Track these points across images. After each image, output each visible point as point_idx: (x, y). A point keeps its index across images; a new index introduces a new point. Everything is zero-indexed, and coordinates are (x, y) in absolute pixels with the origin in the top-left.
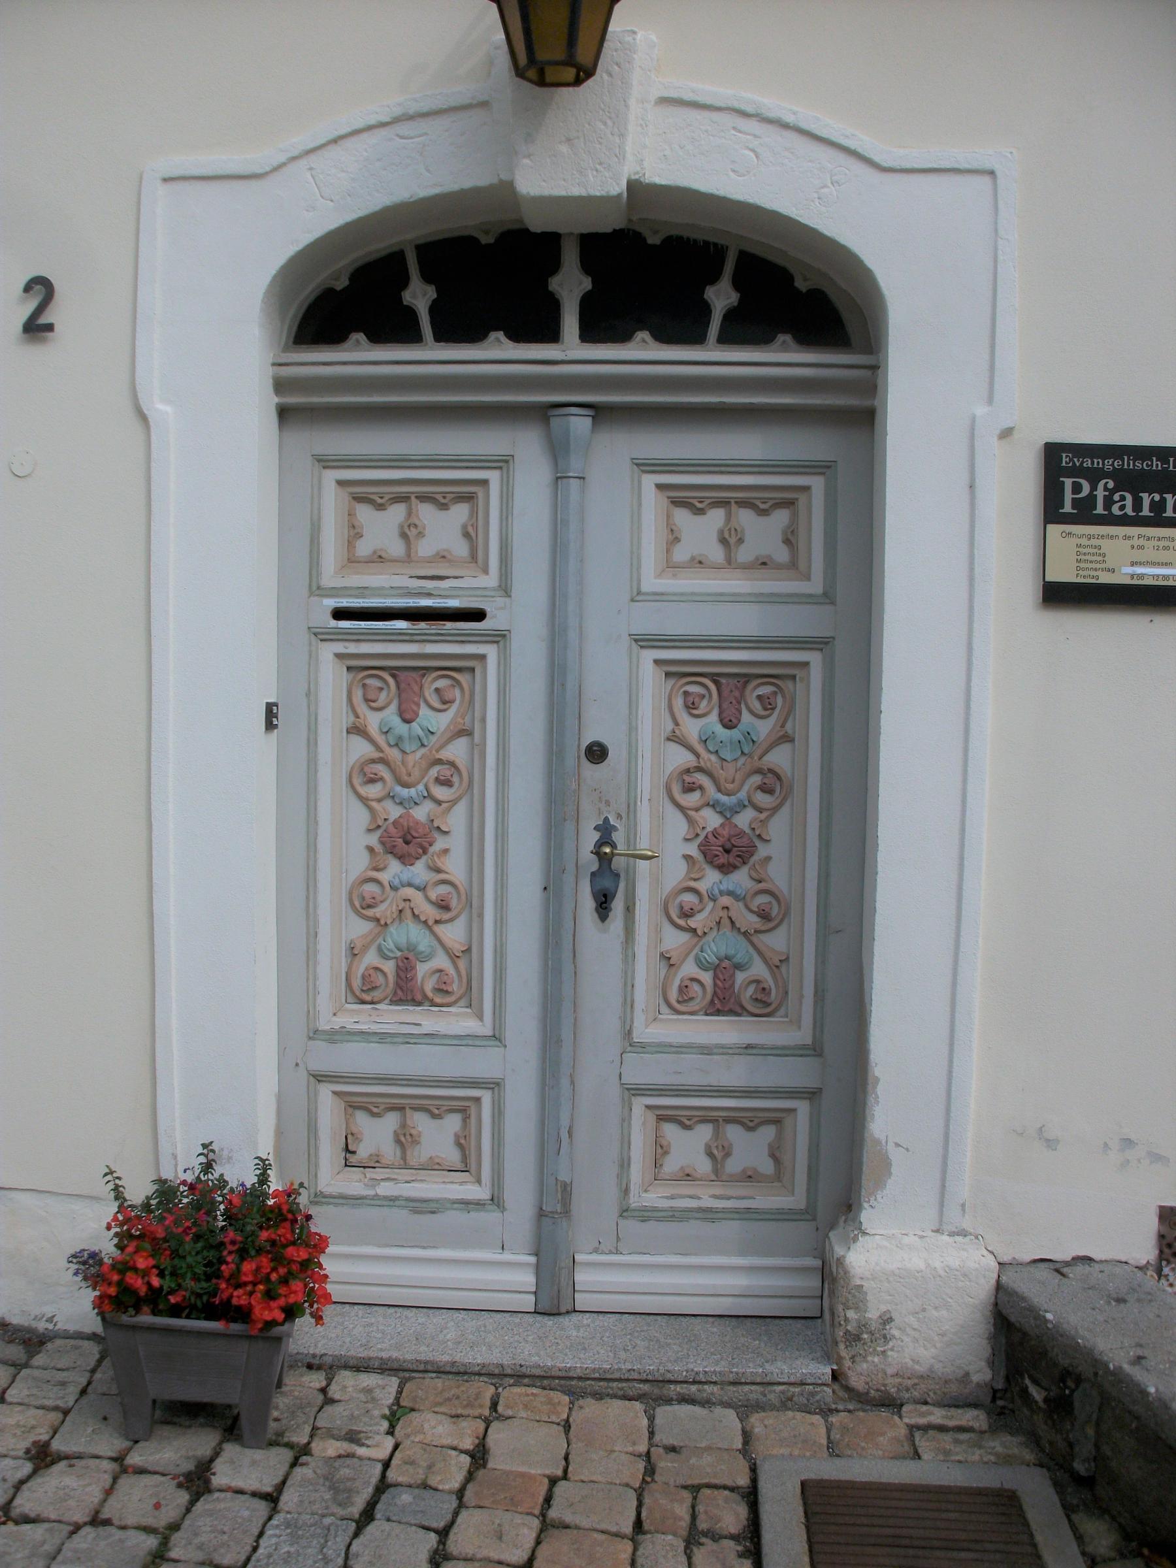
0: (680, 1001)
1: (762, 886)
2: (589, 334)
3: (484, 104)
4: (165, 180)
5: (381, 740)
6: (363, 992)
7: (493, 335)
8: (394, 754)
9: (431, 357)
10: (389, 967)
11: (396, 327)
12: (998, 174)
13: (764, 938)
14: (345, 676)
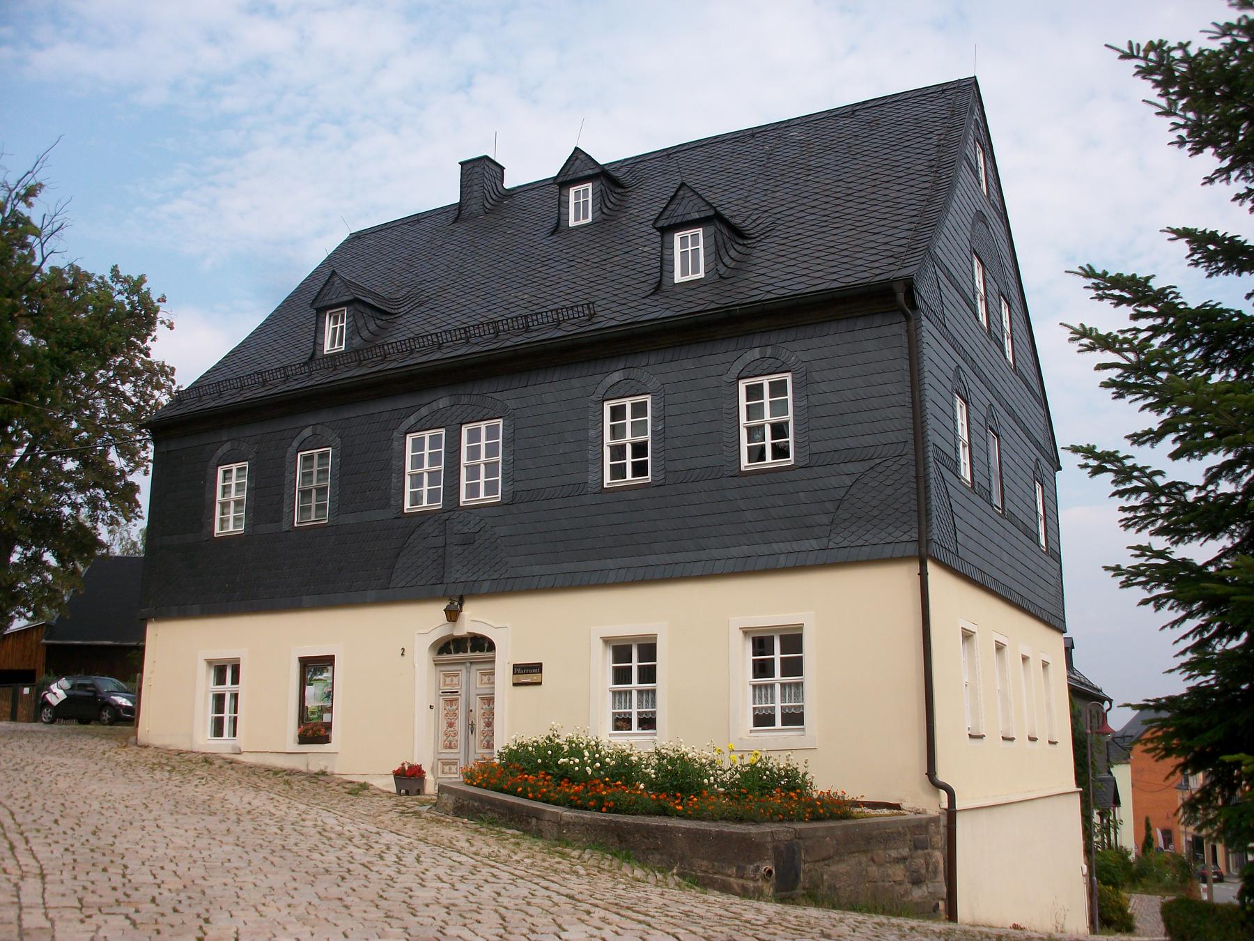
6: (446, 747)
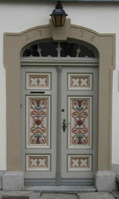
0: (74, 142)
1: (84, 127)
2: (61, 56)
3: (49, 27)
4: (6, 35)
5: (35, 109)
7: (86, 56)
8: (37, 111)
9: (40, 59)
10: (36, 139)
11: (36, 54)
12: (114, 36)
13: (85, 134)
14: (30, 101)
